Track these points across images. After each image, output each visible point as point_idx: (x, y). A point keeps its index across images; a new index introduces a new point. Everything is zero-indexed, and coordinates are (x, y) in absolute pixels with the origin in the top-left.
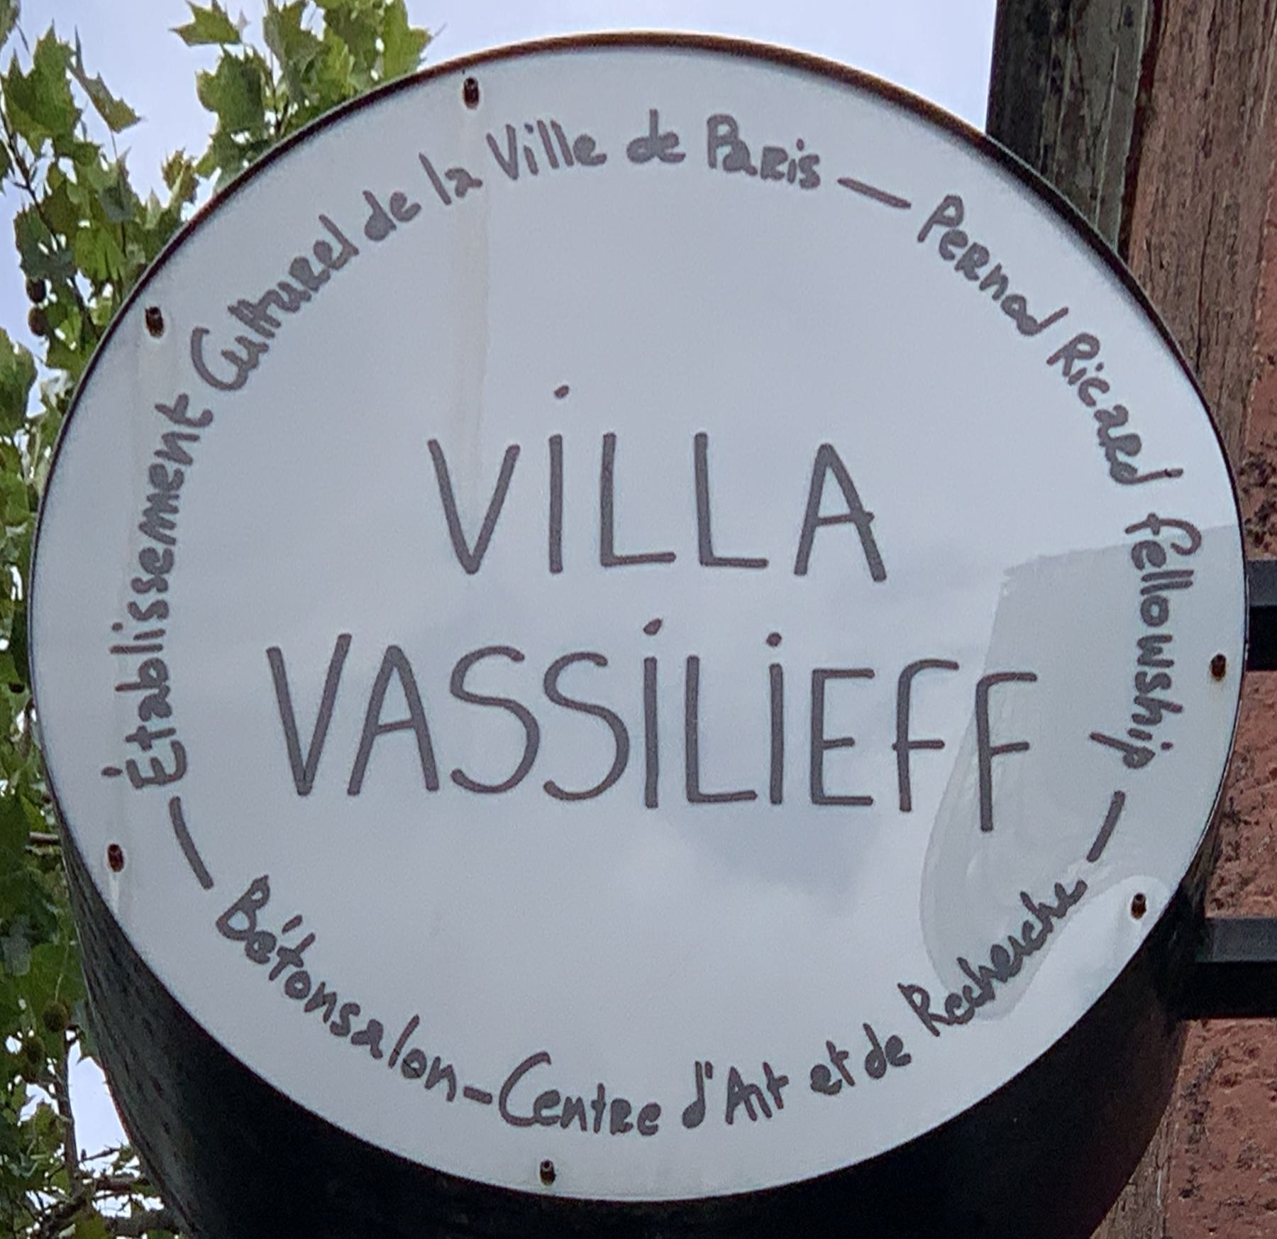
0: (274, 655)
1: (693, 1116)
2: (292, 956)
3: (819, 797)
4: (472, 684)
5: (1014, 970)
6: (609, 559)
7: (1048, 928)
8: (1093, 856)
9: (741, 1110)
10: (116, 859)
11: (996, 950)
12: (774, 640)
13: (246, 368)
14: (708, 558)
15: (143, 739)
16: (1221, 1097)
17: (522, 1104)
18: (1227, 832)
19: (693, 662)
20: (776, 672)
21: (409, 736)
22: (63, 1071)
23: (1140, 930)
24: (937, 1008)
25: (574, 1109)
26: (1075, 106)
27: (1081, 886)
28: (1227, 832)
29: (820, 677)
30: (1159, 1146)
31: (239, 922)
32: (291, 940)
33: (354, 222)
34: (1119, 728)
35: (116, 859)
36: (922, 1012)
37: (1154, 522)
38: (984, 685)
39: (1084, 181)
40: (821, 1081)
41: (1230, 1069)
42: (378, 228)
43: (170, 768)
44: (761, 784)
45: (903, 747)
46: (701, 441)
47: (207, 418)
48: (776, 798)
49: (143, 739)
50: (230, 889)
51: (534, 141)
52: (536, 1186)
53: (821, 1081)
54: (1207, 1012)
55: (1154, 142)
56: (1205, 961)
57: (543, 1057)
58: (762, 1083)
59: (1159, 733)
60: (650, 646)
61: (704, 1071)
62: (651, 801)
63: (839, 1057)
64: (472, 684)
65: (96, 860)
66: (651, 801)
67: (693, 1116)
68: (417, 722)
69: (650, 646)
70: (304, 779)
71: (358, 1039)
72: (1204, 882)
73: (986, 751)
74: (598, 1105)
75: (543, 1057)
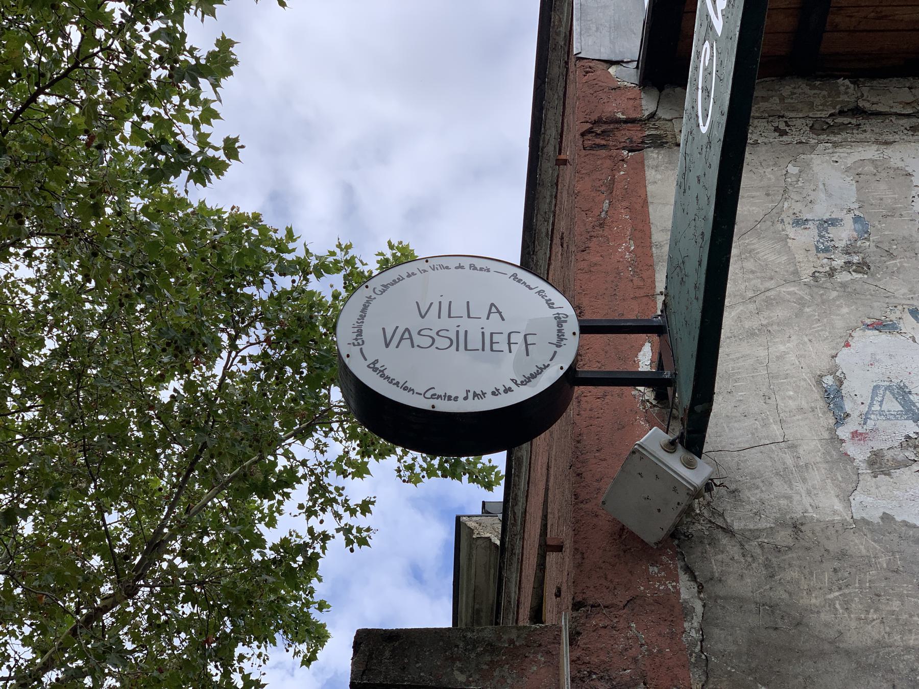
0: (384, 329)
1: (466, 398)
2: (382, 371)
3: (492, 350)
4: (440, 334)
5: (536, 377)
6: (450, 317)
7: (542, 371)
8: (551, 360)
9: (476, 398)
10: (348, 356)
11: (531, 374)
12: (458, 326)
13: (382, 293)
14: (469, 317)
15: (356, 339)
16: (583, 399)
17: (428, 395)
18: (579, 358)
19: (466, 332)
20: (483, 333)
21: (409, 340)
22: (330, 387)
23: (562, 372)
24: (519, 382)
25: (439, 397)
26: (536, 263)
27: (549, 365)
28: (579, 358)
29: (492, 334)
30: (571, 407)
31: (372, 366)
32: (382, 369)
33: (404, 276)
34: (555, 342)
35: (348, 356)
36: (516, 383)
37: (558, 314)
38: (525, 336)
39: (539, 271)
40: (493, 393)
41: (585, 394)
42: (409, 276)
43: (361, 343)
44: (480, 347)
45: (509, 344)
46: (468, 303)
47: (375, 298)
48: (483, 350)
49: (356, 339)
50: (370, 361)
51: (438, 267)
52: (431, 409)
53: (493, 393)
54: (579, 385)
55: (552, 267)
56: (666, 249)
57: (434, 388)
58: (481, 394)
59: (563, 343)
60: (458, 329)
61: (468, 391)
62: (457, 350)
63: (498, 390)
64: (440, 334)
65: (344, 355)
66: (457, 350)
67: (466, 398)
68: (411, 338)
69: (458, 329)
70: (387, 345)
71: (394, 384)
72: (576, 364)
73: (527, 345)
74: (445, 396)
75: (434, 388)
